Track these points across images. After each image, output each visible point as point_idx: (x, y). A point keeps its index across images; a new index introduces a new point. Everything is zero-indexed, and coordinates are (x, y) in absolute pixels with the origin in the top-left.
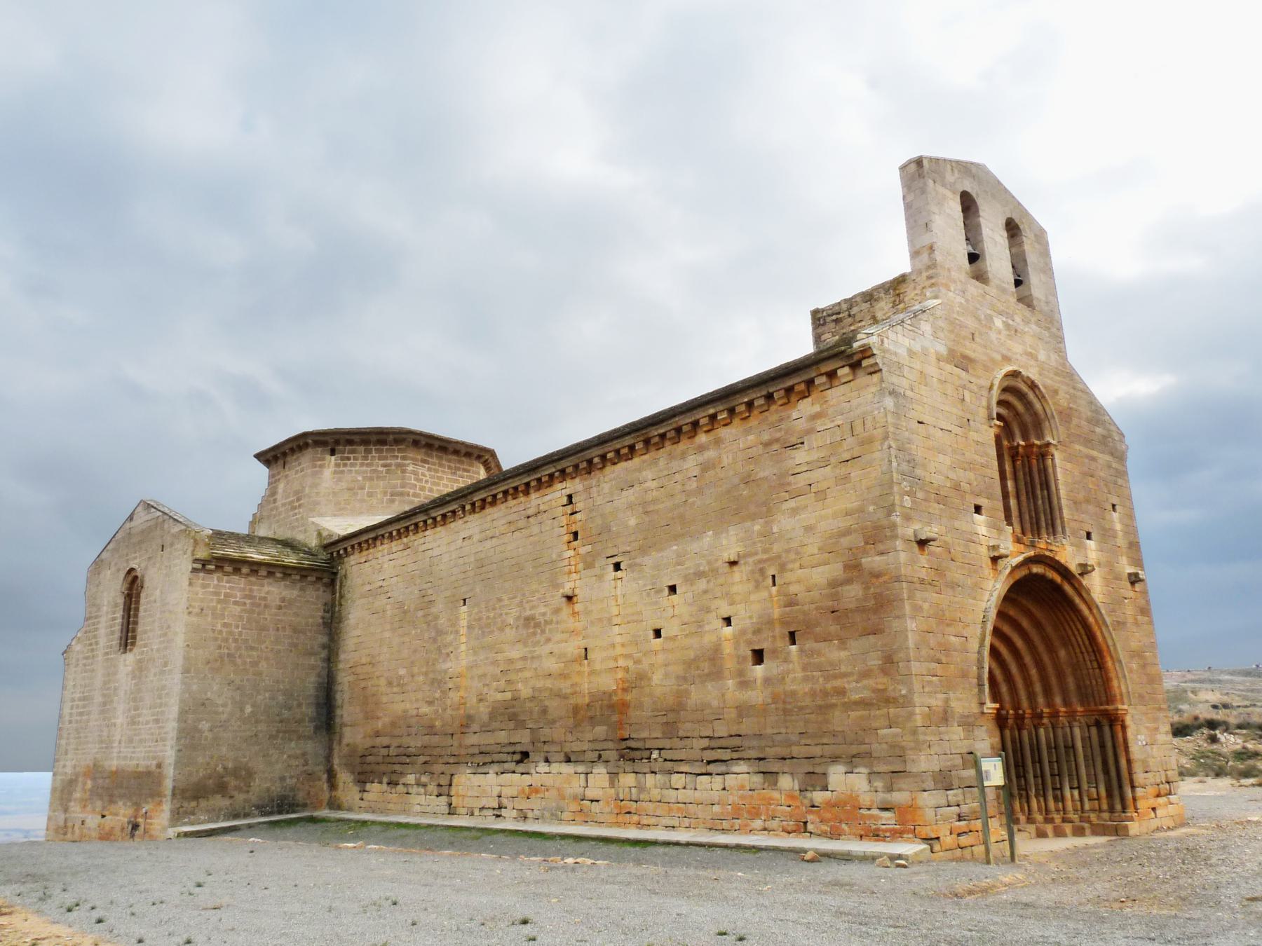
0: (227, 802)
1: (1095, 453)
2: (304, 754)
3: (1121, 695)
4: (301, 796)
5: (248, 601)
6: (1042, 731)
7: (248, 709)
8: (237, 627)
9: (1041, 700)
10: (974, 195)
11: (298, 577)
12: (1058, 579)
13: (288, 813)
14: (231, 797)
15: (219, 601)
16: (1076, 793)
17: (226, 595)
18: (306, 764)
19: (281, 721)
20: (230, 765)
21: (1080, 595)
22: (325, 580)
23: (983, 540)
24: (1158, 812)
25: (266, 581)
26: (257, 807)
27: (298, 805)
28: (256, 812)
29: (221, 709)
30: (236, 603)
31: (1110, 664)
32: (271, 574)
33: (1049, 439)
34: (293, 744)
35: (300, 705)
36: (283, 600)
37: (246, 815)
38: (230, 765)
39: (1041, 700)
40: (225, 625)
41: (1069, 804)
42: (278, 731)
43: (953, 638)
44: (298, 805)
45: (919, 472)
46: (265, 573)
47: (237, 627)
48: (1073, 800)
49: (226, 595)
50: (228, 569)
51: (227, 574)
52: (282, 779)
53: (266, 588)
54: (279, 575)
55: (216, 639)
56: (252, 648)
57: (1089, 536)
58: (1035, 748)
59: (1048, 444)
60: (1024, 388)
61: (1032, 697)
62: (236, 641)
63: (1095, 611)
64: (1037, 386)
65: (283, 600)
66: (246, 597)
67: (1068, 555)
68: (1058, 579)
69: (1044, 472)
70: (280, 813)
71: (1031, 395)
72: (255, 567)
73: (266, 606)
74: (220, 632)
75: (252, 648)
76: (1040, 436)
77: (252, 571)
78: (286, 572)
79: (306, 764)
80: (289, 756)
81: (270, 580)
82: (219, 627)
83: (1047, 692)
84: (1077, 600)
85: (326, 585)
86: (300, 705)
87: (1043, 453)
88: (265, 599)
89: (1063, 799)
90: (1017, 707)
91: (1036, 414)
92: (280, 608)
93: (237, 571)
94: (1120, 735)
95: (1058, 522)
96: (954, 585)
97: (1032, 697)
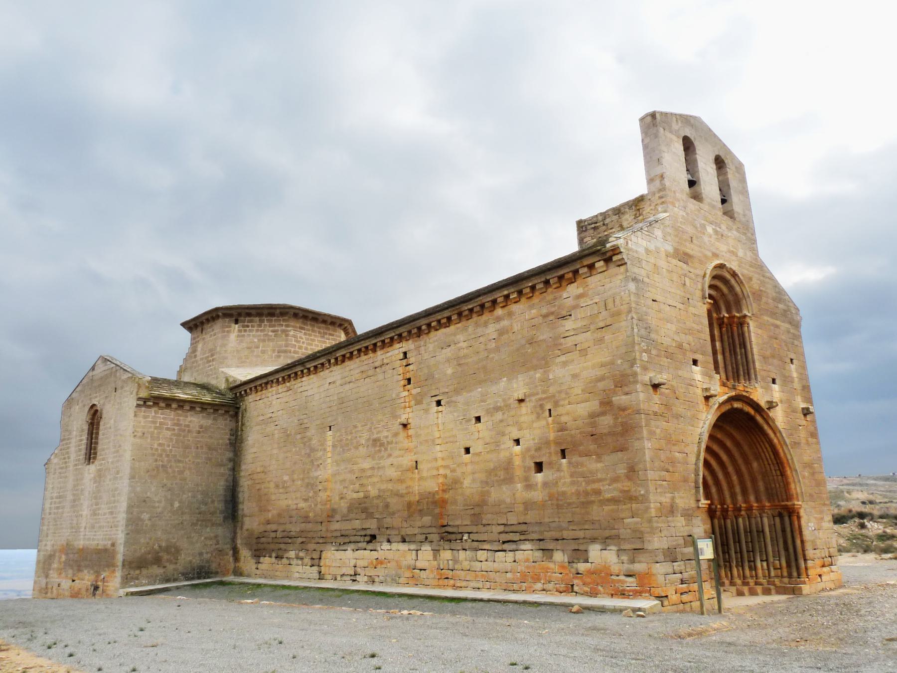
0: (161, 571)
1: (778, 323)
2: (216, 537)
3: (797, 494)
4: (214, 566)
5: (176, 428)
6: (740, 520)
7: (177, 505)
8: (169, 446)
9: (740, 498)
10: (692, 139)
11: (212, 411)
12: (752, 412)
13: (204, 578)
14: (165, 567)
15: (156, 428)
16: (765, 564)
17: (161, 423)
18: (218, 543)
19: (200, 513)
20: (164, 544)
21: (768, 424)
22: (231, 413)
23: (699, 384)
24: (823, 578)
25: (189, 413)
26: (183, 574)
27: (212, 573)
28: (182, 578)
29: (157, 505)
30: (168, 429)
31: (789, 472)
32: (192, 408)
33: (745, 312)
34: (208, 530)
35: (213, 502)
36: (201, 427)
37: (175, 580)
38: (164, 544)
39: (740, 498)
40: (160, 445)
41: (760, 572)
42: (198, 520)
43: (677, 454)
44: (212, 573)
45: (653, 336)
46: (188, 408)
47: (169, 446)
48: (763, 569)
49: (161, 423)
50: (162, 404)
51: (161, 408)
52: (201, 554)
53: (189, 419)
54: (198, 409)
55: (153, 455)
56: (179, 461)
57: (774, 381)
58: (736, 532)
59: (745, 316)
60: (728, 276)
61: (733, 496)
62: (168, 456)
63: (778, 435)
64: (737, 275)
65: (201, 427)
66: (175, 424)
67: (759, 395)
68: (752, 412)
69: (742, 335)
70: (199, 578)
71: (733, 281)
72: (181, 404)
73: (189, 431)
74: (157, 450)
75: (179, 461)
76: (739, 310)
77: (179, 406)
78: (204, 407)
79: (218, 543)
80: (205, 538)
81: (192, 413)
82: (156, 446)
83: (744, 492)
84: (766, 427)
85: (232, 416)
86: (213, 502)
87: (742, 322)
88: (188, 426)
89: (756, 568)
90: (723, 503)
91: (736, 295)
92: (199, 432)
93: (168, 406)
94: (796, 523)
95: (752, 371)
96: (678, 416)
97: (733, 496)
